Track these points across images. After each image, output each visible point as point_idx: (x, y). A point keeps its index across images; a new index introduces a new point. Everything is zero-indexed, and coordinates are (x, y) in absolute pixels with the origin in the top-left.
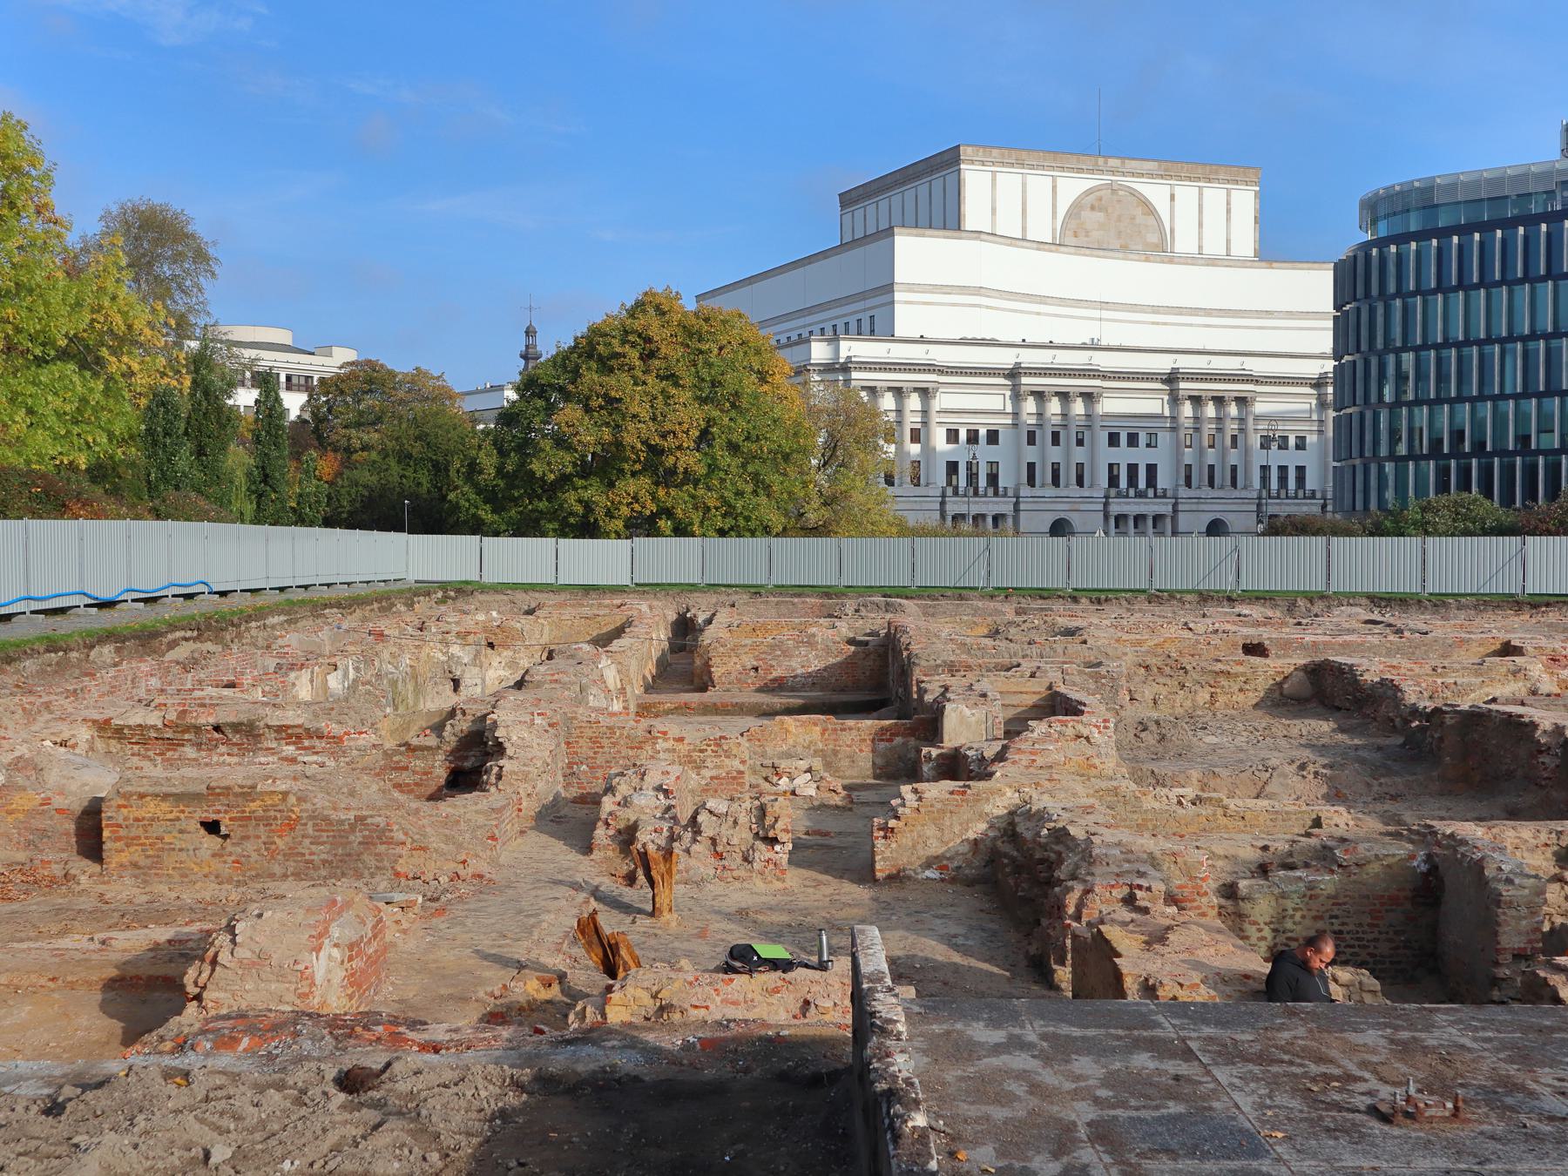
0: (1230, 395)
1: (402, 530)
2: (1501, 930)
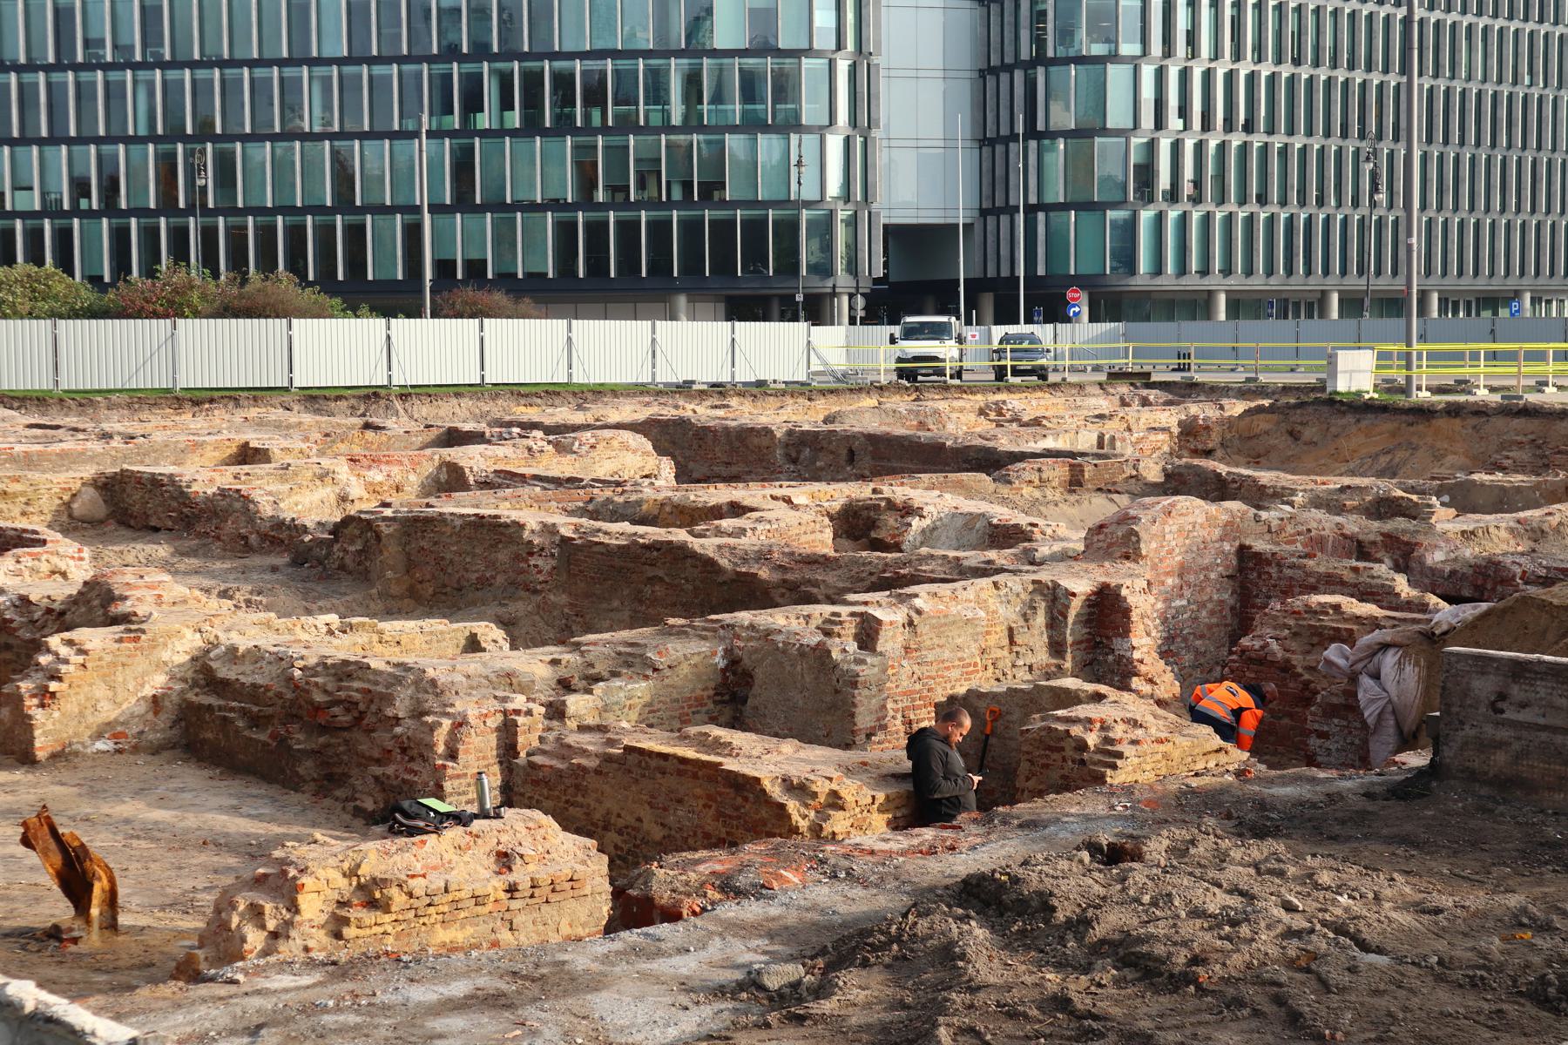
2: (857, 711)
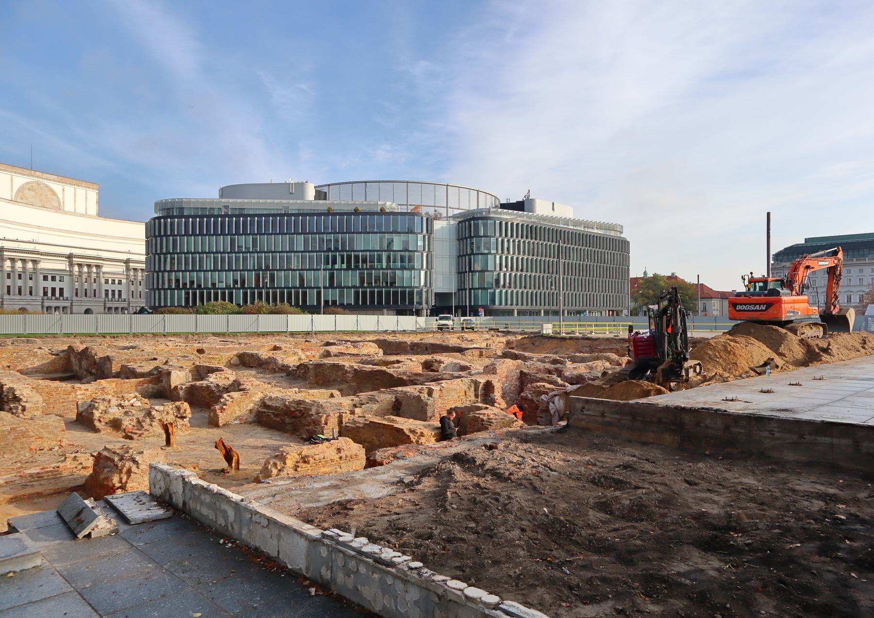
0: (94, 264)
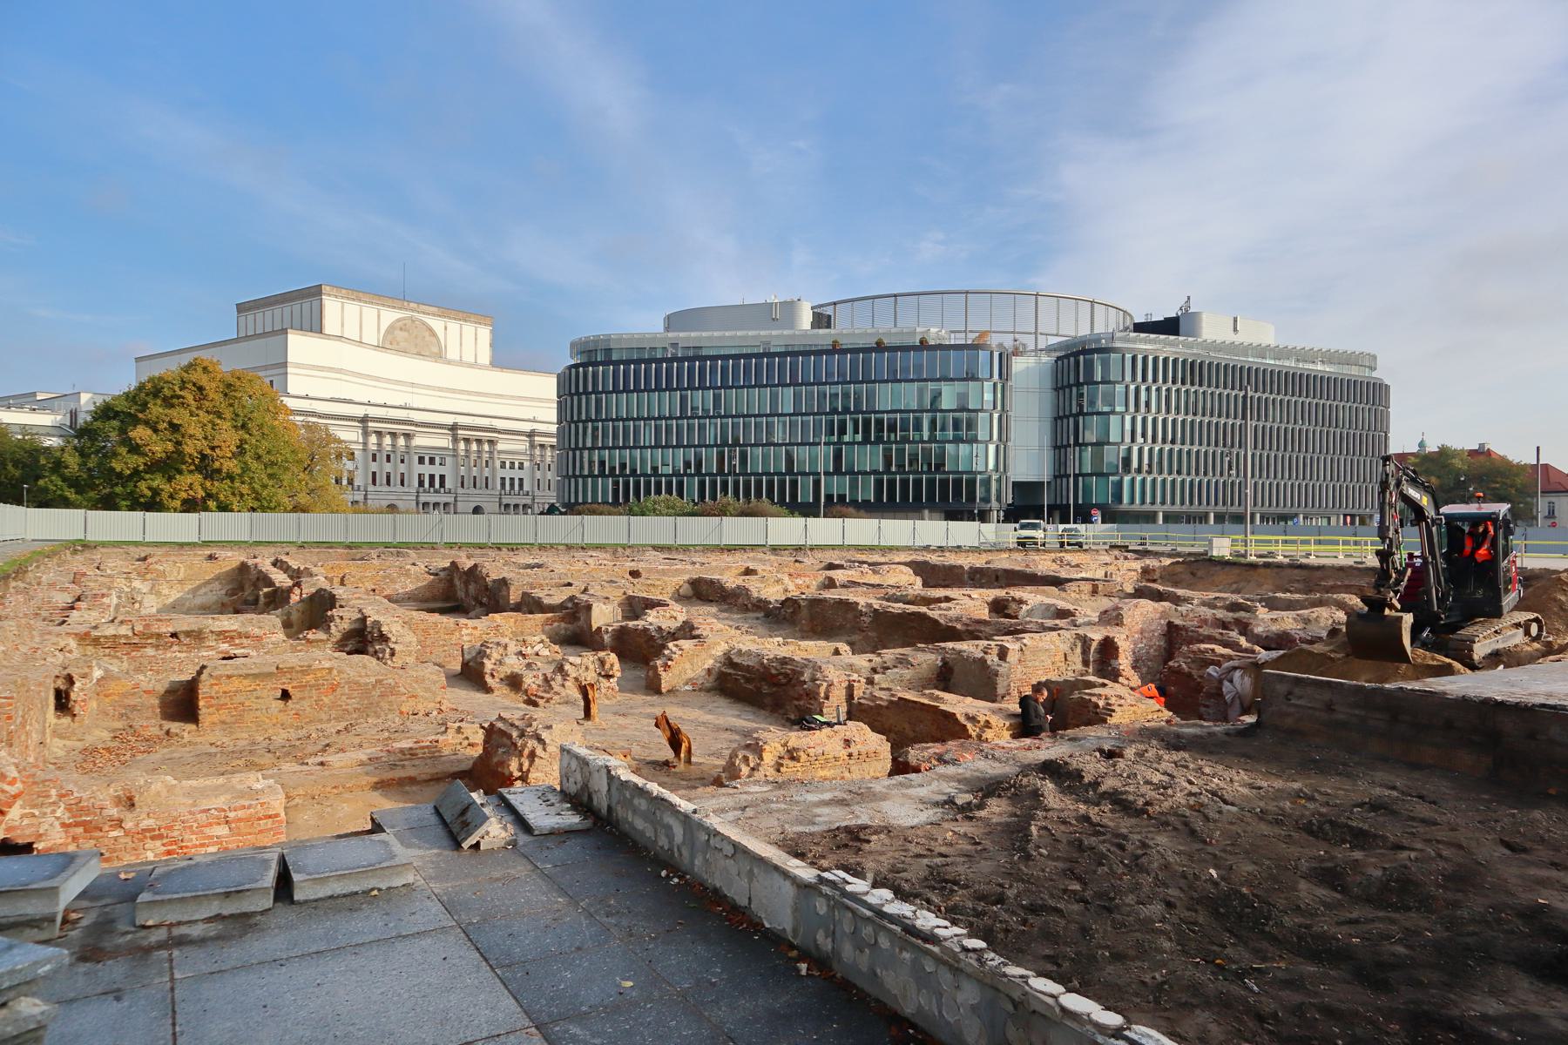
1: (19, 502)
